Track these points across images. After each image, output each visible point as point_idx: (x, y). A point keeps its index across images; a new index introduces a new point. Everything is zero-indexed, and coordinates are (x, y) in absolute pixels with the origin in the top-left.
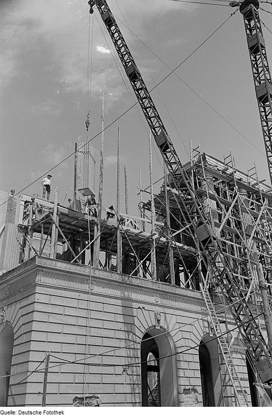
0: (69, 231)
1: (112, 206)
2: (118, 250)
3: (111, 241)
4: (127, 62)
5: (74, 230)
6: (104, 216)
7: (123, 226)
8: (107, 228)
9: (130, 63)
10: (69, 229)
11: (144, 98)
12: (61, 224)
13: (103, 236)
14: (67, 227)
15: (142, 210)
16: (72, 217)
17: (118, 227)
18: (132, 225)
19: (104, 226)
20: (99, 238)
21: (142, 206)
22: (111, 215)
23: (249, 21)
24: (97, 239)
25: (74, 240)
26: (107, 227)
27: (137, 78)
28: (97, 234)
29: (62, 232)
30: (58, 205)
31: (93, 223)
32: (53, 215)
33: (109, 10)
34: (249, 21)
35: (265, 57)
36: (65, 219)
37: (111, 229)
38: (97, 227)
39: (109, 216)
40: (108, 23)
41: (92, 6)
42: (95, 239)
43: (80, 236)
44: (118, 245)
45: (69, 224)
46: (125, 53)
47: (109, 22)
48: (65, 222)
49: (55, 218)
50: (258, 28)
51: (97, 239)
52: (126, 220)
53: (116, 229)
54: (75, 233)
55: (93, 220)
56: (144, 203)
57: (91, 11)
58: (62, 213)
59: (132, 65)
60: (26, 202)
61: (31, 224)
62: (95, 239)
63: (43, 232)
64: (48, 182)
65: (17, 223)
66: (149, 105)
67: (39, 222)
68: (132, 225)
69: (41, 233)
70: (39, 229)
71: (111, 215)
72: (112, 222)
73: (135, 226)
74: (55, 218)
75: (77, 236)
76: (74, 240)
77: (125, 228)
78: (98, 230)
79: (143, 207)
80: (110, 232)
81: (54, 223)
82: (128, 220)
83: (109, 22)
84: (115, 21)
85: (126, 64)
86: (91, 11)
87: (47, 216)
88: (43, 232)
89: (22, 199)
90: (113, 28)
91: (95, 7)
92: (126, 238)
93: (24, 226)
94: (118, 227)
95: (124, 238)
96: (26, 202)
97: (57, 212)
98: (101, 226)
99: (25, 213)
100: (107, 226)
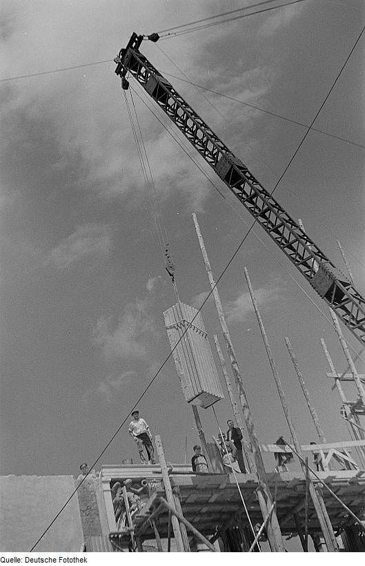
0: (212, 518)
1: (281, 439)
2: (324, 528)
3: (303, 510)
4: (215, 154)
5: (221, 513)
6: (271, 465)
7: (317, 473)
8: (285, 488)
9: (220, 154)
10: (209, 513)
11: (266, 211)
12: (187, 509)
13: (283, 506)
14: (204, 510)
15: (352, 420)
16: (206, 488)
17: (307, 478)
18: (339, 460)
19: (277, 487)
20: (274, 516)
21: (348, 412)
22: (284, 458)
23: (164, 100)
24: (270, 519)
25: (227, 531)
26: (284, 487)
27: (240, 177)
28: (268, 508)
29: (191, 522)
30: (170, 472)
31: (250, 488)
32: (165, 497)
33: (156, 72)
34: (164, 100)
35: (322, 258)
36: (193, 497)
37: (294, 488)
38: (263, 493)
39: (281, 459)
40: (158, 97)
41: (123, 75)
42: (265, 521)
43: (236, 521)
44: (320, 517)
45: (207, 503)
46: (205, 139)
47: (161, 92)
48: (196, 503)
49: (172, 503)
50: (201, 125)
51: (270, 519)
52: (323, 456)
53: (305, 483)
54: (224, 517)
55: (249, 482)
56: (351, 404)
57: (126, 85)
58: (183, 488)
59: (224, 156)
60: (112, 483)
61: (132, 527)
62: (265, 521)
63: (157, 534)
64: (140, 426)
65: (106, 533)
66: (279, 222)
67: (147, 518)
68: (339, 460)
69: (155, 538)
70: (149, 532)
71: (284, 458)
72: (291, 473)
73: (346, 461)
74: (172, 503)
75: (231, 522)
76: (227, 531)
77: (323, 475)
78: (265, 498)
79: (353, 412)
80: (294, 494)
81: (172, 513)
82: (326, 454)
83: (161, 92)
84: (170, 88)
85: (214, 158)
86: (126, 85)
87: (157, 503)
88: (157, 534)
89: (103, 479)
90: (171, 101)
91: (129, 76)
92: (332, 495)
93: (120, 534)
94: (307, 478)
95: (327, 497)
96: (112, 483)
97: (172, 487)
98: (272, 488)
99: (116, 505)
100: (282, 485)
